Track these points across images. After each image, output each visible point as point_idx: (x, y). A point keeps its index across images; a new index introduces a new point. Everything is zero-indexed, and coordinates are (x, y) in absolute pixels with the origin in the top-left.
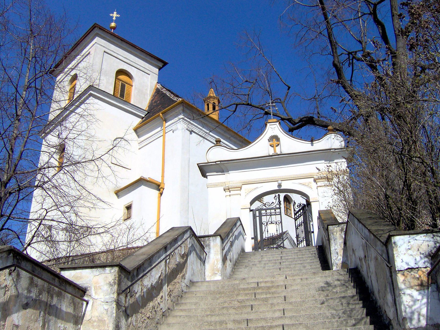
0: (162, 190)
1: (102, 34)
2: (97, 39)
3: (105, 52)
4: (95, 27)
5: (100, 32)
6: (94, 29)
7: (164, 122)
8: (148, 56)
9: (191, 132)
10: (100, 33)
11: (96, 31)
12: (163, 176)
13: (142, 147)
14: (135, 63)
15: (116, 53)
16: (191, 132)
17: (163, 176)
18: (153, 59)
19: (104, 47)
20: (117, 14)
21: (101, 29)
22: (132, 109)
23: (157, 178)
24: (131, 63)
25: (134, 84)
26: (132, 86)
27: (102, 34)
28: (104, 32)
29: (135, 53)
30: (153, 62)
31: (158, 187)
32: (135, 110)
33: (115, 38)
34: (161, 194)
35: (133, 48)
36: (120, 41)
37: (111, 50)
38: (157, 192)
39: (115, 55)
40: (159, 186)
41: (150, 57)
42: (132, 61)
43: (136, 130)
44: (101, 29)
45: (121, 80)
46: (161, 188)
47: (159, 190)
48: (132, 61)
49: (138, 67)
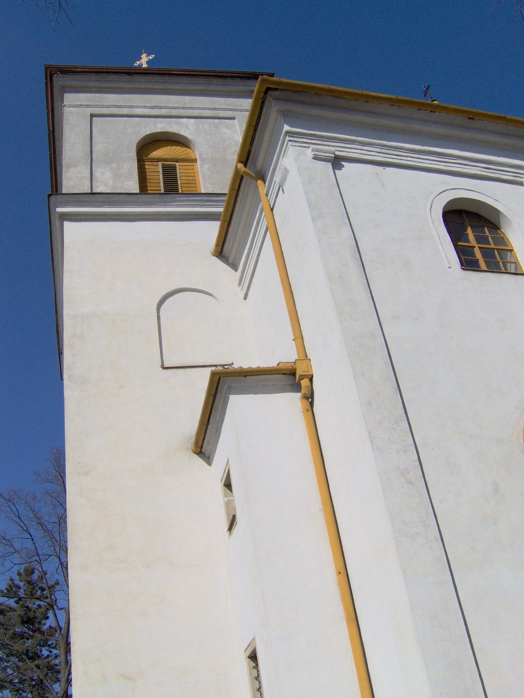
0: (305, 383)
1: (74, 83)
2: (69, 98)
3: (92, 116)
4: (52, 75)
5: (69, 80)
6: (51, 79)
7: (260, 182)
8: (215, 81)
9: (337, 162)
10: (68, 83)
11: (59, 80)
12: (299, 337)
13: (249, 287)
14: (184, 108)
15: (124, 107)
16: (337, 162)
17: (299, 337)
18: (229, 81)
19: (87, 106)
20: (148, 55)
21: (65, 71)
22: (193, 206)
23: (202, 381)
24: (174, 112)
25: (198, 157)
26: (195, 161)
27: (74, 83)
28: (78, 77)
29: (178, 87)
30: (232, 88)
31: (292, 378)
32: (202, 206)
33: (111, 77)
34: (310, 398)
35: (167, 78)
36: (127, 77)
37: (108, 107)
38: (292, 401)
39: (125, 111)
40: (293, 373)
41: (221, 81)
42: (174, 108)
43: (220, 252)
44: (65, 71)
45: (158, 160)
46: (302, 377)
47: (297, 388)
48: (174, 108)
49: (196, 113)
